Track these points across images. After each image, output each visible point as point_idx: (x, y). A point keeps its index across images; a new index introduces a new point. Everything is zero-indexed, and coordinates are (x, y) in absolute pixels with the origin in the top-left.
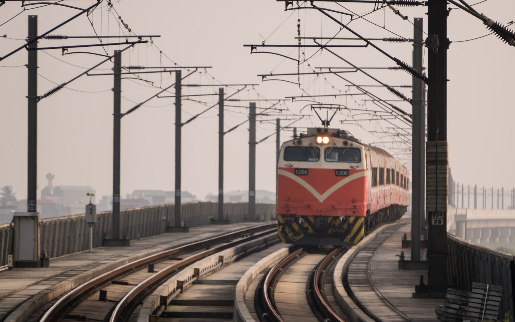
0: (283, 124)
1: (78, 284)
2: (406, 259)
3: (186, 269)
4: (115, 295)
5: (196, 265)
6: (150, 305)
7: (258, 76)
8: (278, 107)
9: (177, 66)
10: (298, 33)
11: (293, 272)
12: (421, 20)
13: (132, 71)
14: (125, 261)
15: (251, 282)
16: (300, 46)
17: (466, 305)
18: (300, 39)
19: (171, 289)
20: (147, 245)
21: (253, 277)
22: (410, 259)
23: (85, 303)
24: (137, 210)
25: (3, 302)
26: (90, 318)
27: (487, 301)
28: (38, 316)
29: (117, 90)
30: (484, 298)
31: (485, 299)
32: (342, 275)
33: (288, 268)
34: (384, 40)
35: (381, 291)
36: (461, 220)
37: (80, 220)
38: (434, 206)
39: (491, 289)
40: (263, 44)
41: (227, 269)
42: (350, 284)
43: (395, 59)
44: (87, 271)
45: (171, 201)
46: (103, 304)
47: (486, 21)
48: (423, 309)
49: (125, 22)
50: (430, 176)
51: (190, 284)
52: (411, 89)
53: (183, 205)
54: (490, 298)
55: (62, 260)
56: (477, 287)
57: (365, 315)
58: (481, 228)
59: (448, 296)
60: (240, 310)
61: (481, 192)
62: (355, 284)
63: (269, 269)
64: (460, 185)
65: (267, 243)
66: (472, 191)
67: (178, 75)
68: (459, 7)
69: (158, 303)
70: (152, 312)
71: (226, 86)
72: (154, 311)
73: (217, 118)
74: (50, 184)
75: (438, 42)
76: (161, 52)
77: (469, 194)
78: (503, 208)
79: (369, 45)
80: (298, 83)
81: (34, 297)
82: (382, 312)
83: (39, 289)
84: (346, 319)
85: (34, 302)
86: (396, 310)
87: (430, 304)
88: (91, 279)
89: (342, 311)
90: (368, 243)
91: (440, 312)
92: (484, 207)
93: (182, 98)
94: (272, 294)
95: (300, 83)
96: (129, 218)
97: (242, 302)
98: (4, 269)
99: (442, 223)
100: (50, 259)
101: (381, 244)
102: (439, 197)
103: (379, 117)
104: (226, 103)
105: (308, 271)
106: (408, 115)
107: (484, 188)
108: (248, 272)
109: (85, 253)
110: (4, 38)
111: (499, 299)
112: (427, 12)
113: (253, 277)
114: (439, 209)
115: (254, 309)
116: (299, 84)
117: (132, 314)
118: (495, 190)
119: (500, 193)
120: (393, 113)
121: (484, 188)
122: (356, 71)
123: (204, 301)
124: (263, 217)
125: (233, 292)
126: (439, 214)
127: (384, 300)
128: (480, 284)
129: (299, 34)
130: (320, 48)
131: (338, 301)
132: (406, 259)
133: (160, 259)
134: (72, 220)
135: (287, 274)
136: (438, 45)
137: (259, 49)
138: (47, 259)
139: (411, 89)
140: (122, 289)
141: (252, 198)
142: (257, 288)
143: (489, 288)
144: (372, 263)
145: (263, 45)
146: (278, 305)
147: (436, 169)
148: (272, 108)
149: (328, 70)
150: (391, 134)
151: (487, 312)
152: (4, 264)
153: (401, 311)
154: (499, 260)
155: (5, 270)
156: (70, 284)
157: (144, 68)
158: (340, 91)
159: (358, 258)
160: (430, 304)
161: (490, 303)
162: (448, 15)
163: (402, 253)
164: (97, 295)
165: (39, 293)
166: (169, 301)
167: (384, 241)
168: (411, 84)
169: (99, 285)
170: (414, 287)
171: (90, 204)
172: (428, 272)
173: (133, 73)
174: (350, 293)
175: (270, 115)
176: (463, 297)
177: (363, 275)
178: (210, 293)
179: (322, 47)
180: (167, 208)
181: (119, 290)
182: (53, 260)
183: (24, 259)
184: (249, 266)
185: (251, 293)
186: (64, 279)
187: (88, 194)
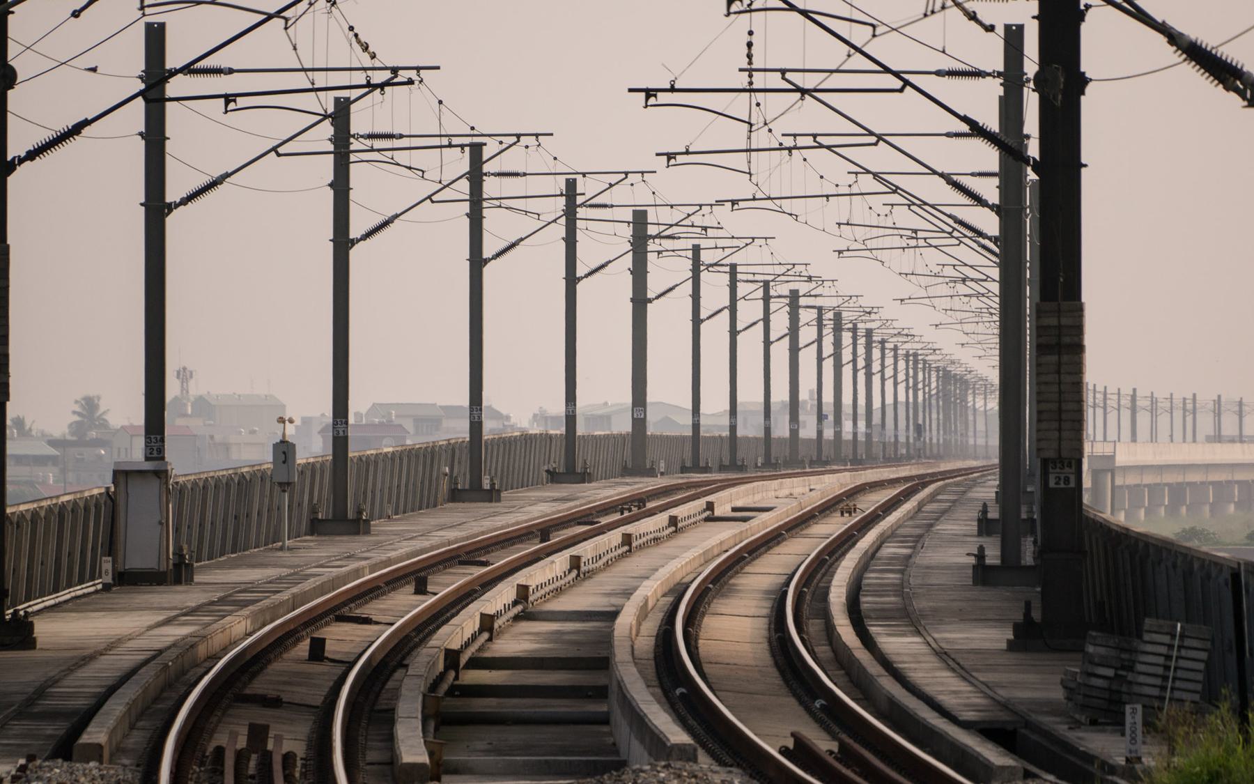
0: (706, 257)
1: (261, 620)
2: (988, 561)
4: (346, 648)
5: (520, 578)
6: (423, 670)
7: (658, 155)
8: (697, 220)
9: (475, 132)
10: (748, 60)
11: (739, 591)
12: (1020, 28)
13: (378, 144)
15: (646, 616)
17: (1131, 669)
18: (751, 72)
19: (468, 634)
20: (408, 531)
21: (650, 604)
22: (997, 562)
24: (386, 454)
25: (97, 666)
26: (291, 701)
27: (1176, 661)
29: (341, 187)
30: (1170, 653)
31: (1172, 657)
32: (847, 600)
33: (726, 583)
34: (939, 73)
35: (936, 636)
37: (258, 477)
39: (1186, 634)
40: (672, 86)
41: (588, 586)
42: (865, 620)
43: (965, 119)
44: (278, 592)
47: (1173, 37)
48: (1032, 678)
49: (363, 38)
51: (508, 621)
52: (996, 181)
54: (1183, 653)
55: (221, 566)
56: (1155, 629)
57: (904, 691)
58: (1145, 486)
59: (1091, 649)
60: (626, 682)
61: (1147, 403)
62: (877, 619)
63: (684, 586)
64: (1100, 388)
66: (1126, 402)
67: (476, 150)
68: (1104, 3)
69: (441, 667)
70: (428, 685)
71: (584, 175)
72: (431, 684)
73: (562, 246)
75: (1062, 80)
76: (440, 102)
77: (1119, 410)
78: (1194, 441)
79: (908, 88)
80: (748, 171)
81: (164, 654)
82: (942, 684)
83: (175, 636)
84: (861, 699)
85: (166, 666)
86: (971, 679)
87: (1048, 665)
89: (852, 681)
90: (899, 525)
91: (1072, 685)
92: (1153, 438)
93: (485, 204)
94: (693, 643)
95: (752, 172)
96: (367, 471)
97: (628, 662)
98: (92, 589)
99: (1072, 485)
100: (196, 565)
101: (931, 525)
103: (921, 242)
104: (581, 212)
105: (770, 589)
106: (990, 238)
107: (1152, 397)
108: (637, 592)
109: (271, 549)
110: (92, 74)
111: (1204, 655)
113: (650, 604)
114: (1065, 454)
115: (655, 679)
116: (750, 174)
117: (384, 691)
118: (1178, 402)
119: (1189, 406)
120: (956, 234)
121: (1152, 397)
122: (876, 144)
123: (542, 659)
124: (662, 465)
125: (607, 639)
126: (1065, 464)
127: (944, 656)
128: (1161, 622)
129: (750, 63)
130: (798, 95)
131: (842, 661)
132: (988, 561)
133: (440, 563)
134: (243, 476)
135: (724, 596)
136: (1062, 86)
137: (663, 98)
138: (189, 567)
139: (996, 181)
140: (359, 633)
141: (639, 424)
142: (659, 630)
143: (1180, 633)
144: (913, 571)
145: (673, 89)
146: (707, 668)
147: (1059, 364)
148: (683, 223)
149: (809, 141)
150: (947, 280)
151: (1178, 684)
152: (92, 578)
153: (982, 683)
154: (1202, 566)
155: (96, 592)
156: (243, 623)
157: (401, 136)
158: (837, 186)
159: (879, 559)
160: (1048, 665)
161: (1182, 663)
162: (1083, 20)
163: (981, 549)
164: (303, 648)
165: (174, 645)
166: (464, 659)
167: (937, 519)
168: (996, 169)
169: (306, 625)
170: (1011, 625)
171: (283, 442)
172: (1042, 593)
173: (379, 150)
174: (867, 641)
175: (680, 238)
176: (1123, 650)
177: (893, 599)
179: (804, 92)
180: (452, 449)
181: (352, 635)
182: (201, 567)
183: (139, 566)
184: (642, 578)
185: (646, 642)
186: (230, 613)
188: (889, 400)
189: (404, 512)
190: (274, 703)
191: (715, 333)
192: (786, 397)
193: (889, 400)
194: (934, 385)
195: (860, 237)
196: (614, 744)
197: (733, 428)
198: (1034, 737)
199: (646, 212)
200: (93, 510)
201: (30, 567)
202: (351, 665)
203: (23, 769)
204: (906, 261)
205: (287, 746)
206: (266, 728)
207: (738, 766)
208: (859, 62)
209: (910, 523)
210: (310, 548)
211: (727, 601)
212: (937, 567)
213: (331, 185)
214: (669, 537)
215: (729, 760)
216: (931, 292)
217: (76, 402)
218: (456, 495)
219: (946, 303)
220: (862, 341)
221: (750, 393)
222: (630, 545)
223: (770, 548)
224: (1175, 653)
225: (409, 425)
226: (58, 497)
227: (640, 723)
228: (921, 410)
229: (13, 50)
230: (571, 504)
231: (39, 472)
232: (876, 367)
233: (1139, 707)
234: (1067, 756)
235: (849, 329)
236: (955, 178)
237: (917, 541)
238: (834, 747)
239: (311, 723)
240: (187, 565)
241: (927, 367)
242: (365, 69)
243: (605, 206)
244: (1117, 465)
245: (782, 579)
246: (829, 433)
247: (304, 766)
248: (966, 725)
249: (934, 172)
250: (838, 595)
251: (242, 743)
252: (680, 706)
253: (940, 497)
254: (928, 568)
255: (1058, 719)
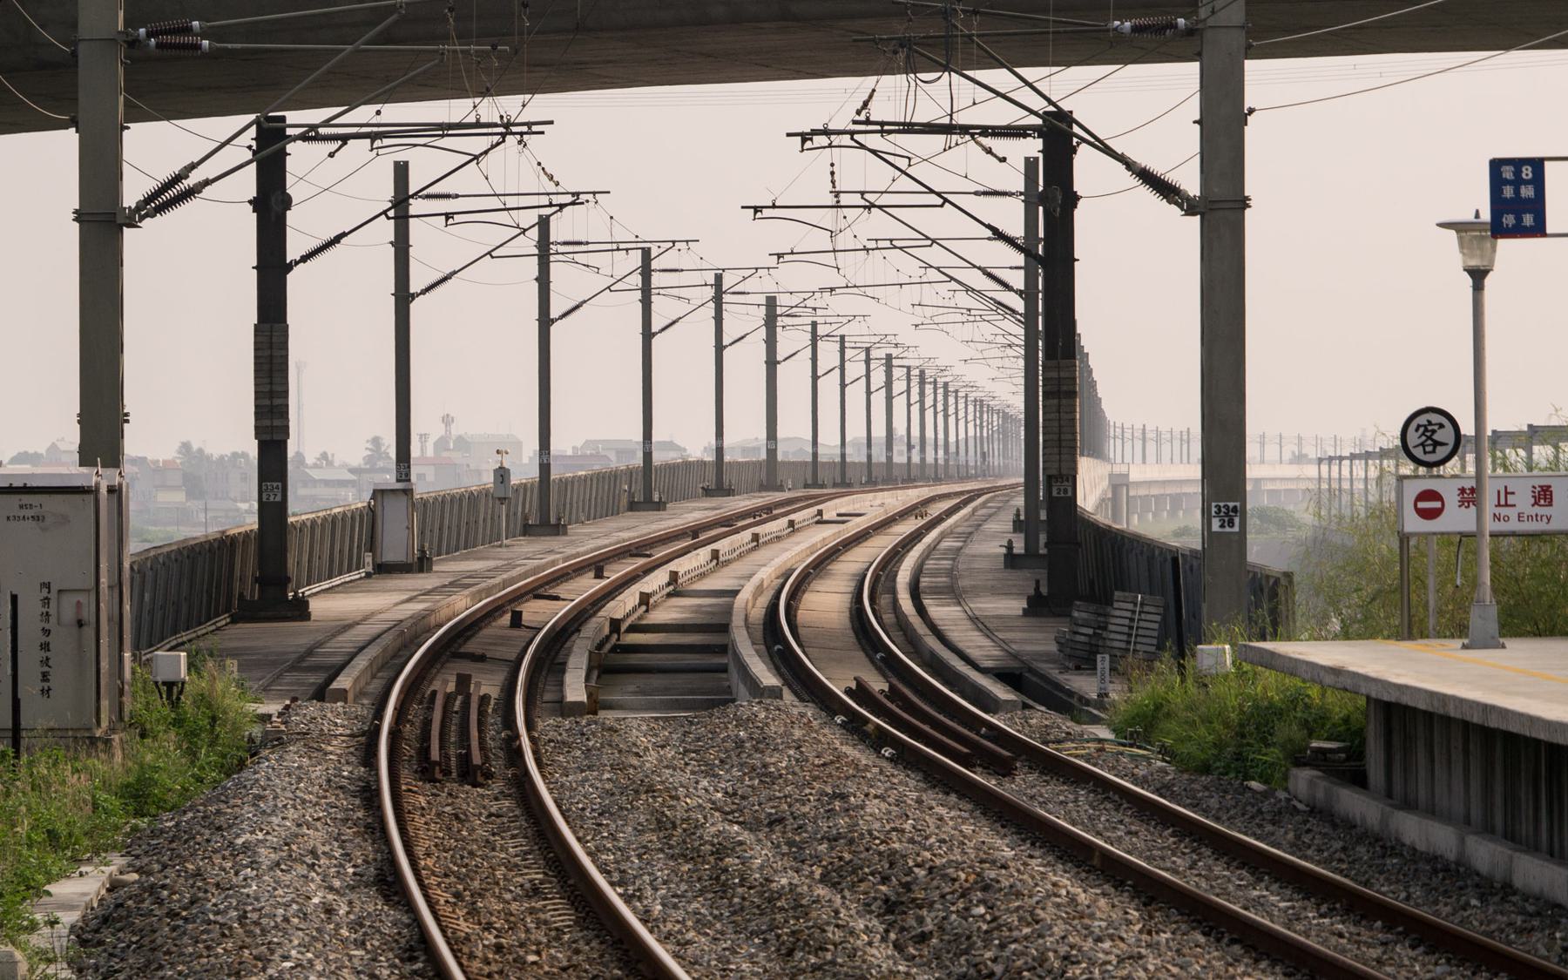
0: (821, 330)
2: (1015, 551)
3: (656, 572)
4: (540, 618)
5: (672, 566)
8: (810, 303)
9: (639, 240)
11: (833, 574)
12: (1036, 159)
14: (558, 560)
15: (762, 592)
16: (838, 206)
17: (1105, 629)
19: (629, 607)
22: (1023, 551)
23: (487, 632)
24: (580, 477)
28: (408, 654)
33: (824, 568)
35: (971, 605)
36: (1119, 484)
38: (1056, 465)
41: (726, 571)
43: (989, 227)
45: (638, 461)
46: (515, 632)
47: (1129, 165)
50: (1048, 416)
53: (656, 467)
54: (1143, 616)
55: (454, 559)
59: (1076, 614)
62: (930, 594)
65: (793, 527)
66: (1138, 434)
67: (646, 254)
69: (607, 631)
74: (448, 431)
76: (612, 218)
79: (947, 204)
82: (971, 641)
88: (500, 591)
90: (956, 525)
91: (1063, 641)
98: (358, 577)
99: (1070, 494)
100: (434, 559)
101: (980, 525)
102: (1064, 451)
103: (978, 318)
104: (726, 298)
111: (1158, 618)
112: (1041, 148)
113: (765, 585)
114: (1064, 472)
118: (1176, 434)
122: (930, 246)
125: (728, 610)
127: (976, 621)
128: (1127, 594)
129: (834, 187)
131: (902, 624)
132: (1015, 551)
135: (821, 578)
138: (429, 560)
141: (772, 452)
144: (961, 559)
146: (801, 631)
149: (887, 244)
151: (1139, 639)
152: (358, 568)
155: (361, 578)
157: (587, 243)
161: (1142, 624)
163: (1010, 542)
164: (508, 617)
166: (624, 627)
168: (1023, 264)
169: (511, 601)
173: (563, 254)
174: (921, 610)
176: (1100, 615)
177: (944, 579)
178: (692, 612)
180: (630, 472)
185: (758, 612)
187: (498, 452)
188: (962, 435)
189: (595, 518)
190: (481, 658)
191: (828, 386)
192: (884, 434)
193: (962, 435)
194: (995, 424)
195: (928, 315)
196: (729, 687)
197: (843, 456)
198: (1034, 679)
199: (775, 297)
200: (358, 518)
201: (310, 561)
202: (540, 629)
203: (287, 707)
204: (968, 331)
205: (484, 690)
206: (469, 677)
207: (813, 702)
208: (905, 183)
209: (965, 524)
210: (522, 545)
211: (822, 581)
212: (980, 556)
213: (536, 279)
214: (789, 535)
215: (807, 697)
216: (986, 354)
217: (368, 441)
218: (633, 506)
219: (999, 363)
220: (940, 391)
221: (856, 431)
222: (758, 541)
223: (860, 543)
224: (1137, 617)
225: (613, 456)
226: (331, 509)
227: (744, 670)
228: (985, 440)
229: (290, 180)
230: (718, 512)
231: (342, 492)
232: (951, 410)
233: (1107, 657)
234: (1056, 692)
235: (930, 383)
236: (989, 270)
237: (967, 537)
238: (886, 687)
239: (505, 674)
240: (428, 559)
241: (991, 410)
242: (548, 194)
243: (743, 293)
244: (1131, 480)
245: (865, 566)
246: (916, 459)
247: (496, 704)
248: (984, 671)
249: (974, 266)
250: (904, 576)
251: (451, 687)
252: (777, 659)
253: (990, 505)
254: (975, 556)
255: (1051, 666)
